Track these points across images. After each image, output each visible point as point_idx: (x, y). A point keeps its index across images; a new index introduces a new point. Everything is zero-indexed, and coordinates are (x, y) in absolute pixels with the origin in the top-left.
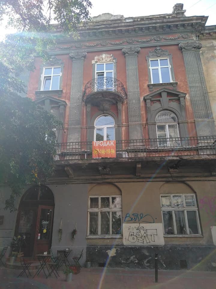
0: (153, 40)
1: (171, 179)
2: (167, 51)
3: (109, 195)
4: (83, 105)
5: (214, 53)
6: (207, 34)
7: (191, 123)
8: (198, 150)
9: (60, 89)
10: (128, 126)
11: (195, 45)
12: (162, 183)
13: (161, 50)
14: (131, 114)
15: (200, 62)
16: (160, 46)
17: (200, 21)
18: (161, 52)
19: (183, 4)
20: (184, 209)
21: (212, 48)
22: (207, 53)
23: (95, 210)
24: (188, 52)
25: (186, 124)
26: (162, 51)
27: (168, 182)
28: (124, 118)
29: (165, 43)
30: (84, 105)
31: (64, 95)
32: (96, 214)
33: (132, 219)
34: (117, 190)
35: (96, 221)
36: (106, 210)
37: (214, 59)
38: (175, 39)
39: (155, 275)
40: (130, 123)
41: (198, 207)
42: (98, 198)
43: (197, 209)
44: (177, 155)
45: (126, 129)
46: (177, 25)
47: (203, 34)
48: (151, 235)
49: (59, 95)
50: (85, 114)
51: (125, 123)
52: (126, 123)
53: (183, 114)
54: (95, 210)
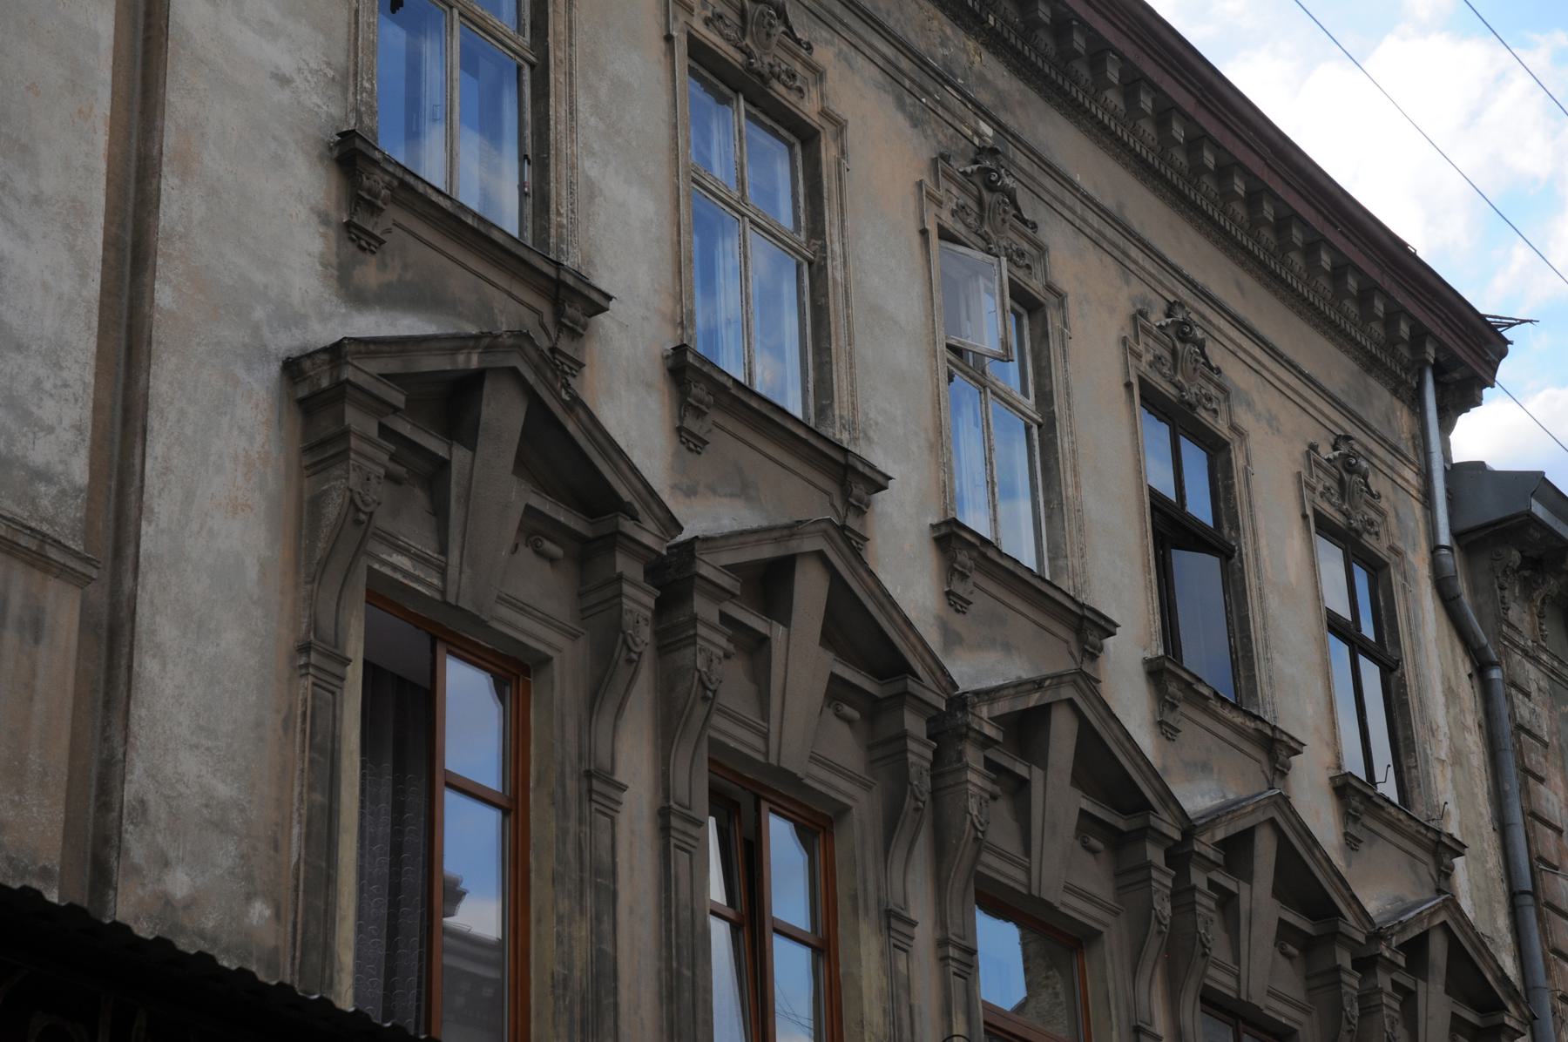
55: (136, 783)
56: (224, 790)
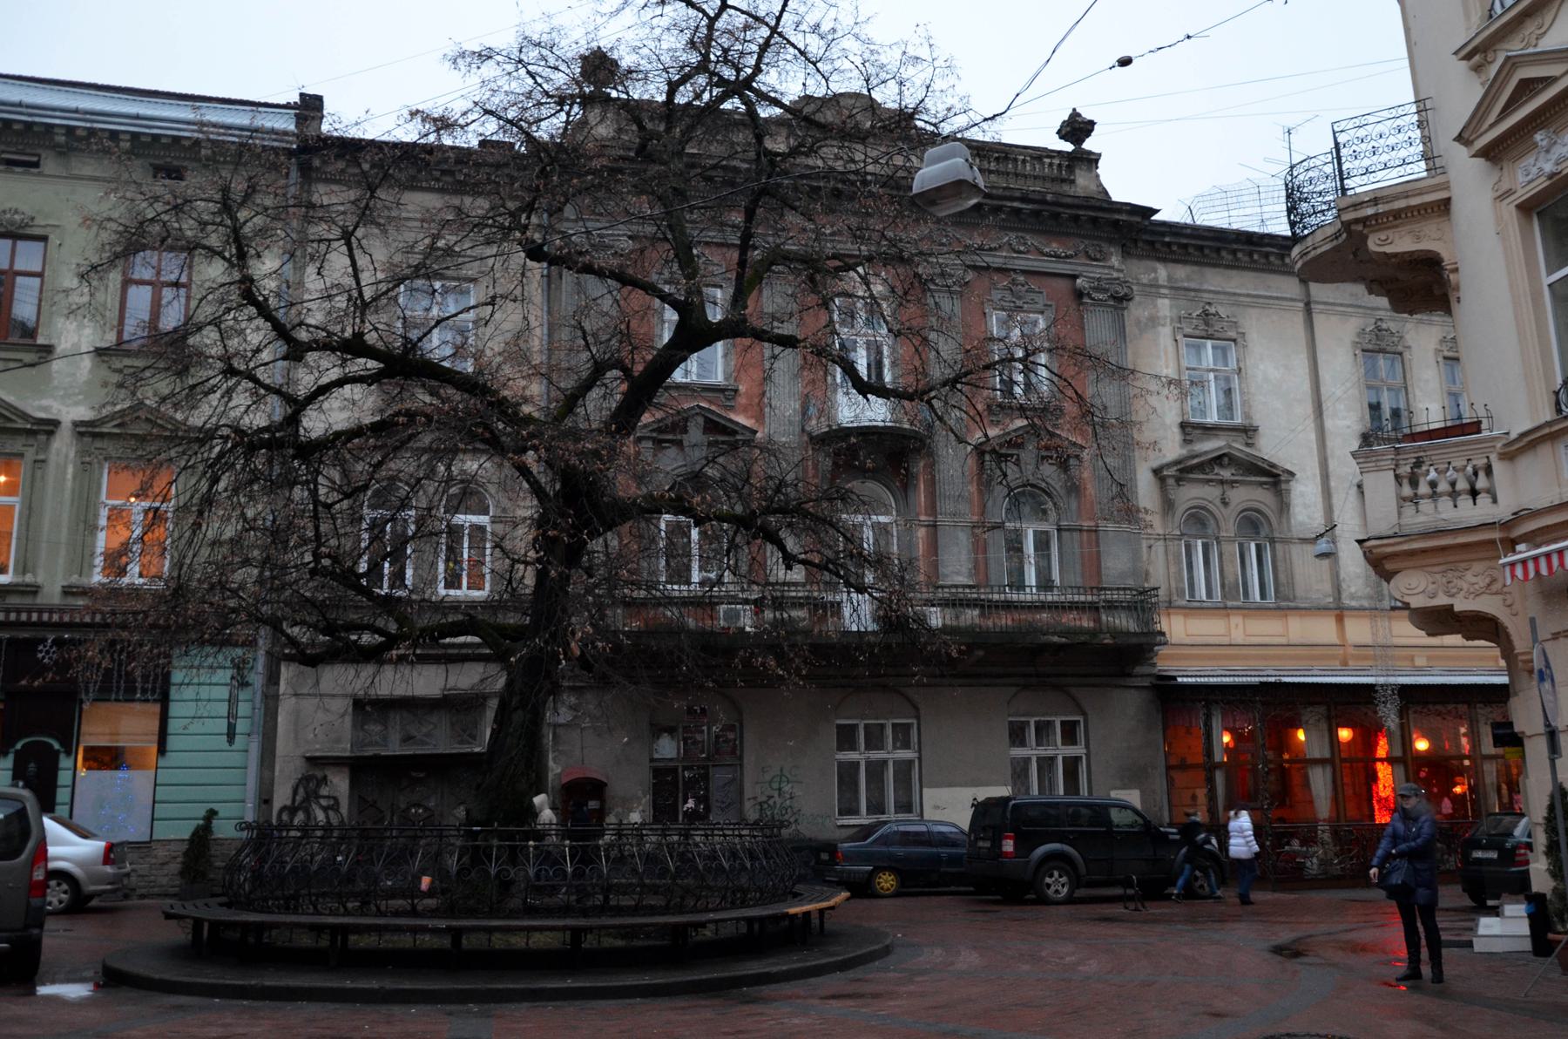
3: (856, 718)
5: (1155, 306)
8: (1097, 609)
9: (726, 379)
10: (935, 526)
12: (1014, 689)
16: (1024, 272)
19: (1092, 123)
21: (1153, 290)
22: (1140, 303)
23: (852, 756)
25: (1076, 535)
26: (1030, 291)
36: (876, 755)
38: (1067, 257)
39: (1161, 732)
40: (940, 518)
43: (916, 755)
47: (1135, 241)
50: (1423, 942)
51: (926, 514)
54: (852, 756)
55: (1342, 575)
56: (1358, 571)
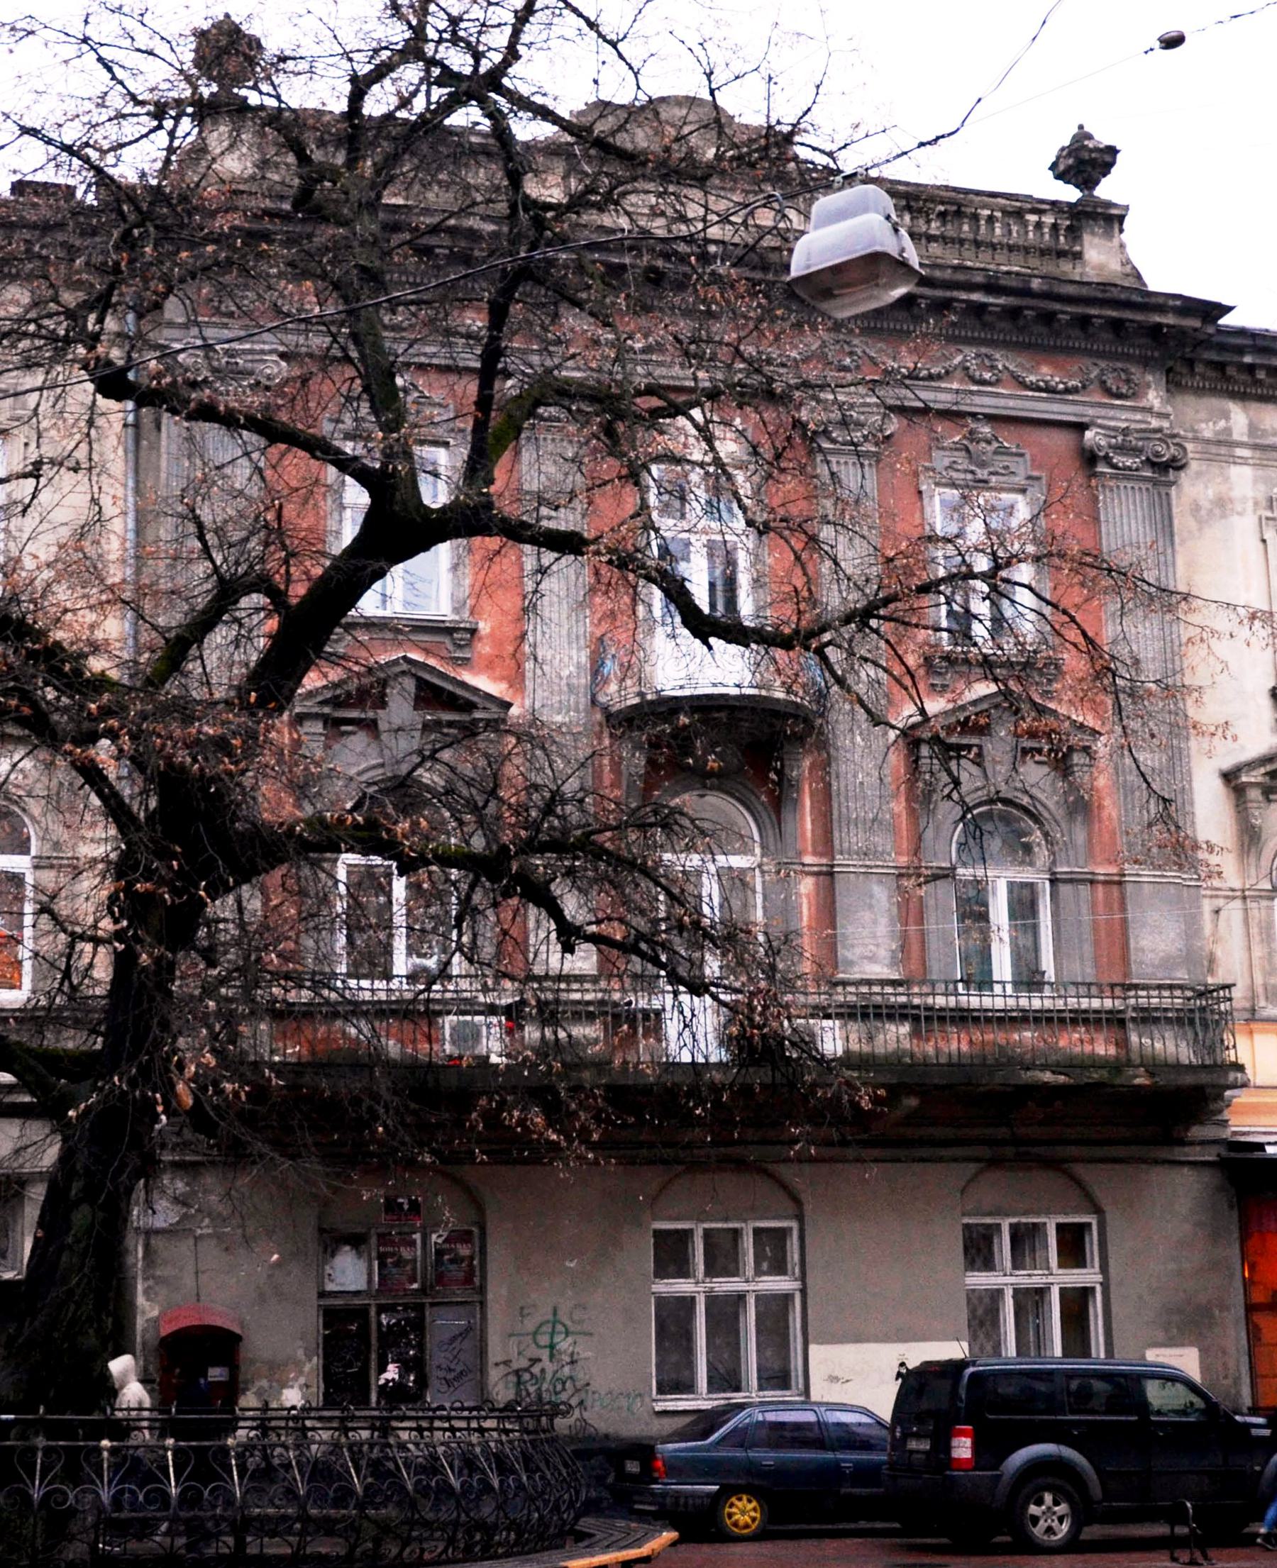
0: (959, 373)
1: (1009, 1151)
2: (1022, 455)
4: (597, 728)
6: (1211, 364)
7: (1106, 883)
8: (1122, 1023)
9: (456, 610)
11: (1157, 455)
12: (972, 1167)
13: (996, 445)
14: (844, 810)
15: (1169, 551)
16: (991, 418)
17: (1196, 323)
18: (996, 453)
20: (1051, 1279)
21: (1223, 450)
23: (682, 1287)
24: (1122, 485)
25: (1084, 890)
27: (994, 1163)
28: (809, 826)
29: (1019, 404)
30: (600, 725)
31: (484, 648)
32: (687, 1303)
33: (116, 269)
34: (790, 1207)
35: (687, 1336)
36: (725, 1285)
37: (1224, 516)
40: (839, 859)
41: (1104, 1269)
42: (688, 1234)
43: (1099, 1278)
44: (913, 669)
45: (817, 884)
46: (1090, 317)
48: (66, 62)
49: (460, 647)
51: (815, 853)
52: (821, 855)
53: (1080, 836)
